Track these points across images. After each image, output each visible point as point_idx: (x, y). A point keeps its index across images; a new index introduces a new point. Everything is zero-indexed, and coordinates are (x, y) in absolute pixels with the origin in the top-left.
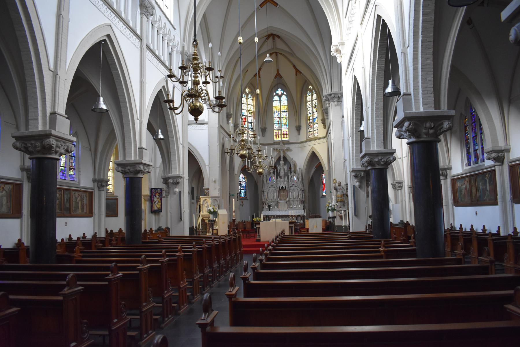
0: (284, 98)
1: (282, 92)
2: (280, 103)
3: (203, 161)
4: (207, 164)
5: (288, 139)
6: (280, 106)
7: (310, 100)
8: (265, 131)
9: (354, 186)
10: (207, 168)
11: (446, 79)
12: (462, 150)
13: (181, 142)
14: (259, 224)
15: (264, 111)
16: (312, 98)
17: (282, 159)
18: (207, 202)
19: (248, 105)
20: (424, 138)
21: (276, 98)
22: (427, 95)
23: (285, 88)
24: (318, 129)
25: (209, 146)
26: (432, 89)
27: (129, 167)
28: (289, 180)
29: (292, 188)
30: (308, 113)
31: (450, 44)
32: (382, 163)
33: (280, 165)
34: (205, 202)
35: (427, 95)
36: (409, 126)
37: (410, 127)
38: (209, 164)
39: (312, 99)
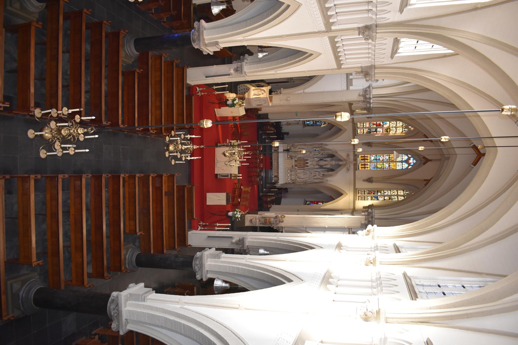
0: (405, 166)
3: (309, 87)
4: (306, 91)
5: (360, 169)
7: (399, 194)
8: (369, 146)
9: (231, 237)
13: (278, 72)
15: (390, 145)
19: (397, 129)
21: (405, 158)
23: (415, 167)
25: (323, 92)
28: (315, 170)
29: (308, 172)
34: (263, 92)
38: (306, 93)
39: (399, 195)
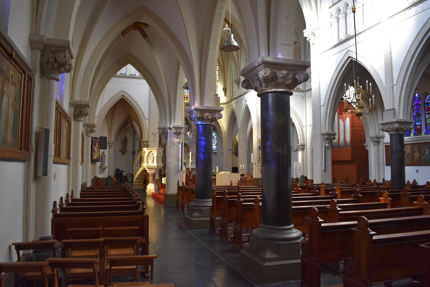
4: (147, 117)
10: (147, 121)
14: (215, 175)
18: (153, 154)
27: (208, 114)
32: (405, 130)
34: (151, 154)
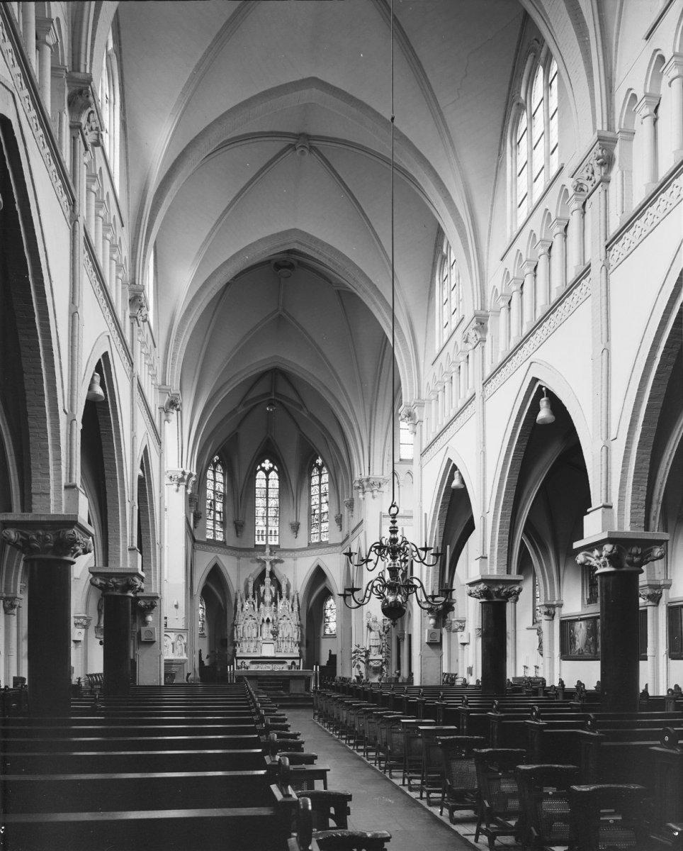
0: (273, 475)
1: (271, 465)
2: (267, 482)
6: (267, 488)
7: (317, 482)
11: (660, 490)
12: (583, 584)
16: (320, 481)
17: (267, 575)
20: (626, 567)
21: (261, 474)
22: (637, 510)
24: (327, 531)
26: (644, 502)
30: (313, 503)
31: (673, 443)
32: (503, 594)
33: (263, 583)
35: (637, 510)
36: (612, 551)
37: (614, 552)
